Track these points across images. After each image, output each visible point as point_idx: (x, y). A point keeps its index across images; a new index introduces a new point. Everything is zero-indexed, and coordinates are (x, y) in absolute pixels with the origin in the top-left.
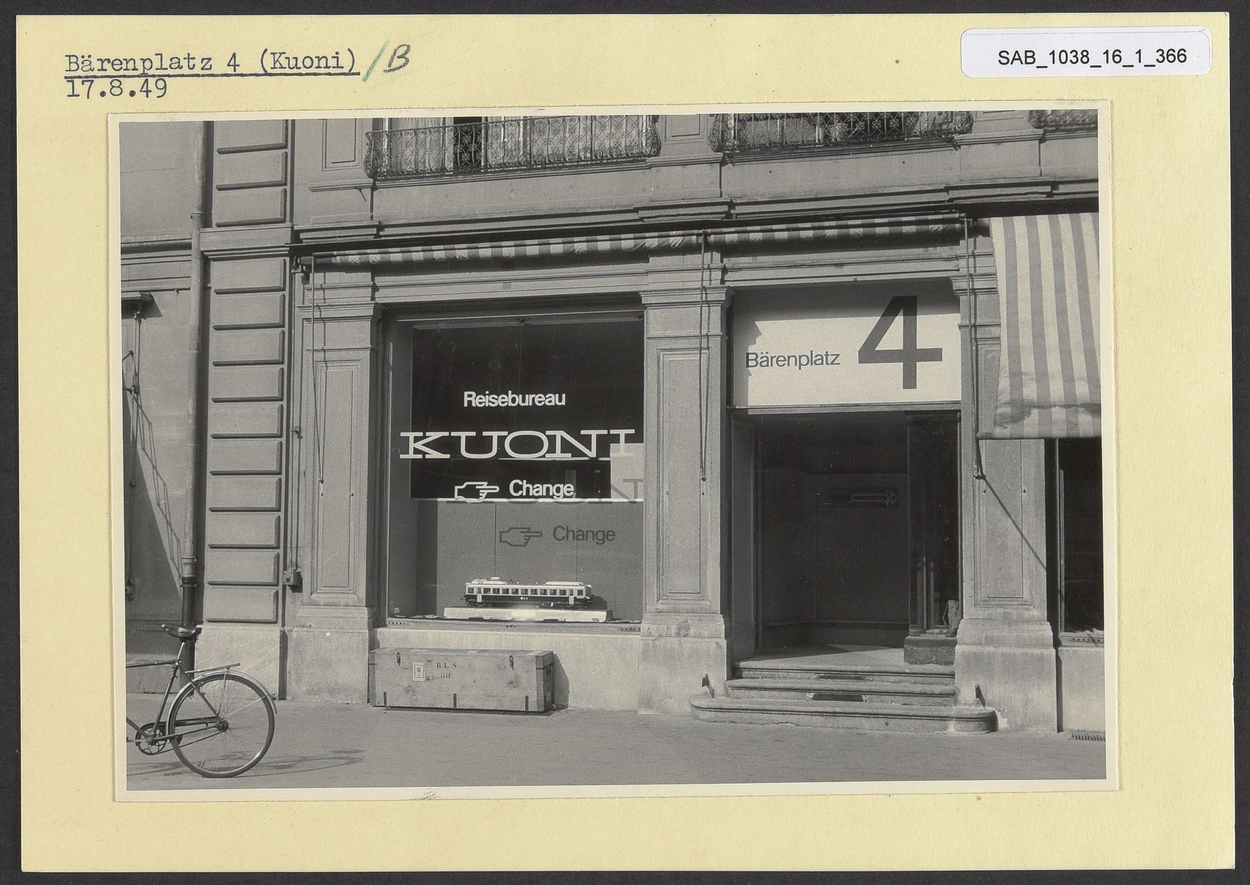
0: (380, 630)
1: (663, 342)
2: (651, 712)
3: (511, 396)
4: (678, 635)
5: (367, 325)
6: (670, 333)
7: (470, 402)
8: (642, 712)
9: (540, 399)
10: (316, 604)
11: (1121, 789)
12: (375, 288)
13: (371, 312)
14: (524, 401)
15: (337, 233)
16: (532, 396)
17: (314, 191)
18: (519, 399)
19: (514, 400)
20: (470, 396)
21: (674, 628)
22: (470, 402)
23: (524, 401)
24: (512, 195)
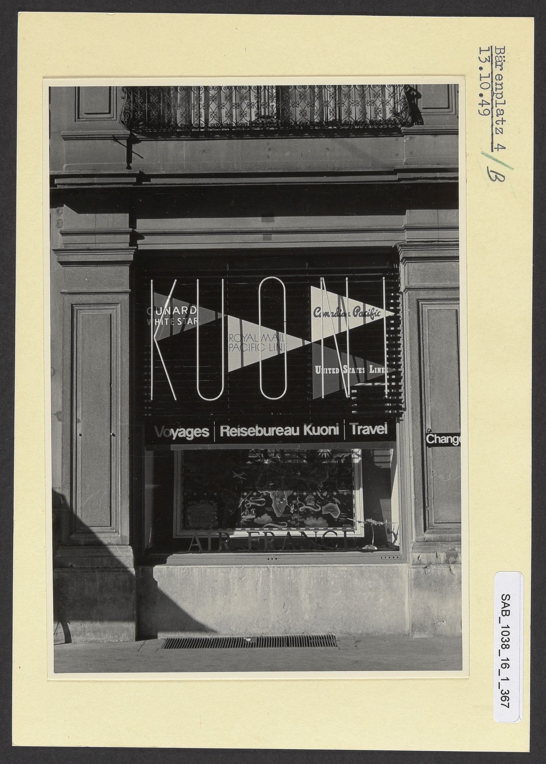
0: (156, 568)
1: (422, 292)
2: (424, 636)
3: (257, 428)
4: (447, 562)
5: (126, 270)
6: (427, 284)
7: (225, 433)
8: (416, 636)
9: (279, 431)
10: (76, 545)
11: (48, 681)
12: (135, 237)
13: (131, 258)
14: (267, 432)
15: (95, 180)
16: (269, 434)
17: (65, 139)
18: (263, 431)
19: (260, 432)
20: (225, 428)
21: (442, 556)
22: (225, 433)
23: (267, 432)
24: (270, 153)
